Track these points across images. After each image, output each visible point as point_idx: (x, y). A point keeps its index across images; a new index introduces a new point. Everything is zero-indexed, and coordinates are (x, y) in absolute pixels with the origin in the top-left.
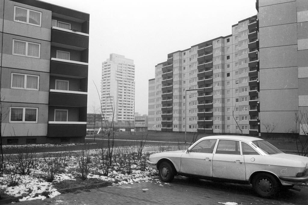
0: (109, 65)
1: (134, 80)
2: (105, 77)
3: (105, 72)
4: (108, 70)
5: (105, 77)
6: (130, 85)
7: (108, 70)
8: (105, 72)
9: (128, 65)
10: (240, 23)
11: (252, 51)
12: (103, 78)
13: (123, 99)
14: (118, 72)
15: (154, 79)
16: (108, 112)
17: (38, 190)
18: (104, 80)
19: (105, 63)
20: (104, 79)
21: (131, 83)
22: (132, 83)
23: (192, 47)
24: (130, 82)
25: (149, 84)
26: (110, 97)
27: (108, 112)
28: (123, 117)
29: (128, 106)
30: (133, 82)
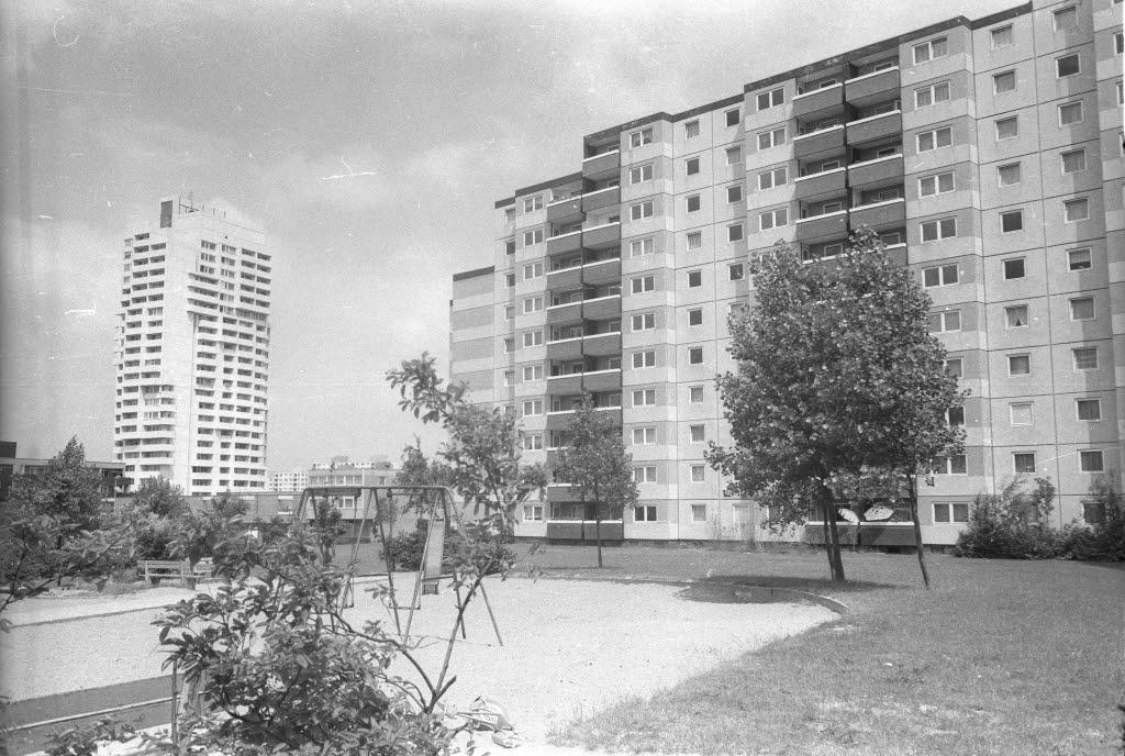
0: (156, 247)
1: (269, 319)
2: (137, 300)
3: (138, 275)
4: (150, 279)
5: (137, 300)
6: (248, 337)
7: (150, 279)
8: (138, 275)
9: (245, 252)
10: (522, 194)
11: (562, 268)
12: (126, 304)
13: (217, 399)
14: (197, 277)
15: (490, 270)
16: (147, 455)
17: (186, 314)
18: (133, 312)
19: (140, 237)
20: (134, 306)
21: (252, 331)
22: (259, 328)
23: (520, 193)
24: (249, 325)
25: (458, 294)
26: (156, 388)
27: (147, 455)
28: (215, 476)
29: (243, 428)
30: (261, 323)
